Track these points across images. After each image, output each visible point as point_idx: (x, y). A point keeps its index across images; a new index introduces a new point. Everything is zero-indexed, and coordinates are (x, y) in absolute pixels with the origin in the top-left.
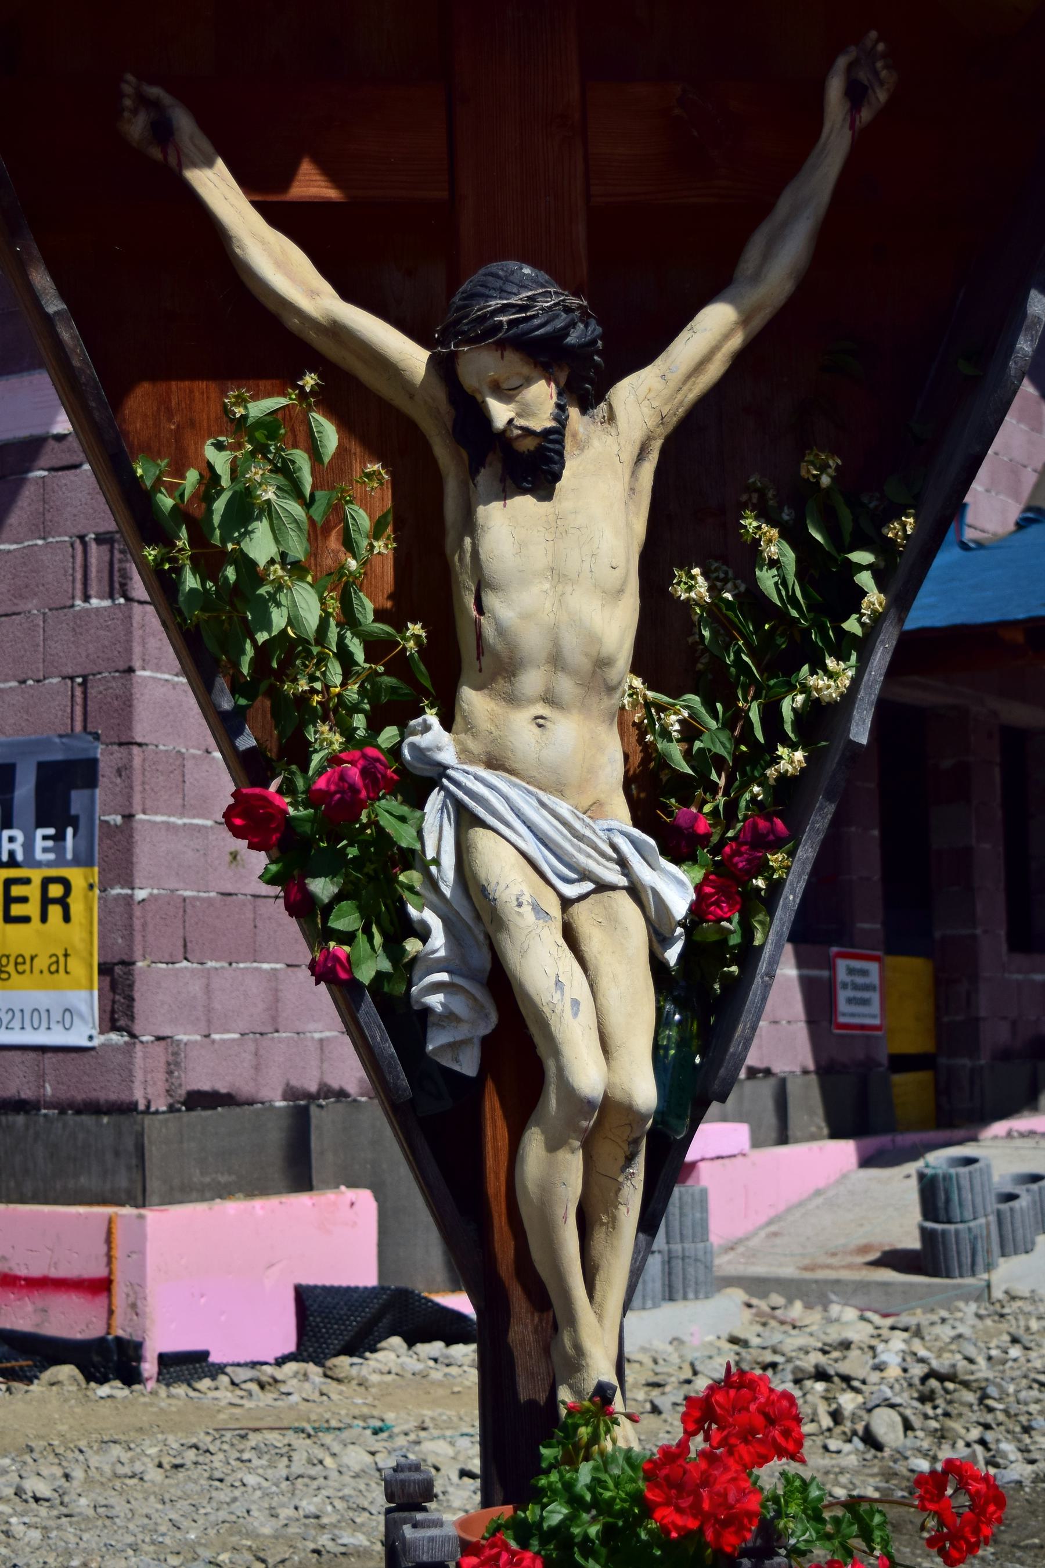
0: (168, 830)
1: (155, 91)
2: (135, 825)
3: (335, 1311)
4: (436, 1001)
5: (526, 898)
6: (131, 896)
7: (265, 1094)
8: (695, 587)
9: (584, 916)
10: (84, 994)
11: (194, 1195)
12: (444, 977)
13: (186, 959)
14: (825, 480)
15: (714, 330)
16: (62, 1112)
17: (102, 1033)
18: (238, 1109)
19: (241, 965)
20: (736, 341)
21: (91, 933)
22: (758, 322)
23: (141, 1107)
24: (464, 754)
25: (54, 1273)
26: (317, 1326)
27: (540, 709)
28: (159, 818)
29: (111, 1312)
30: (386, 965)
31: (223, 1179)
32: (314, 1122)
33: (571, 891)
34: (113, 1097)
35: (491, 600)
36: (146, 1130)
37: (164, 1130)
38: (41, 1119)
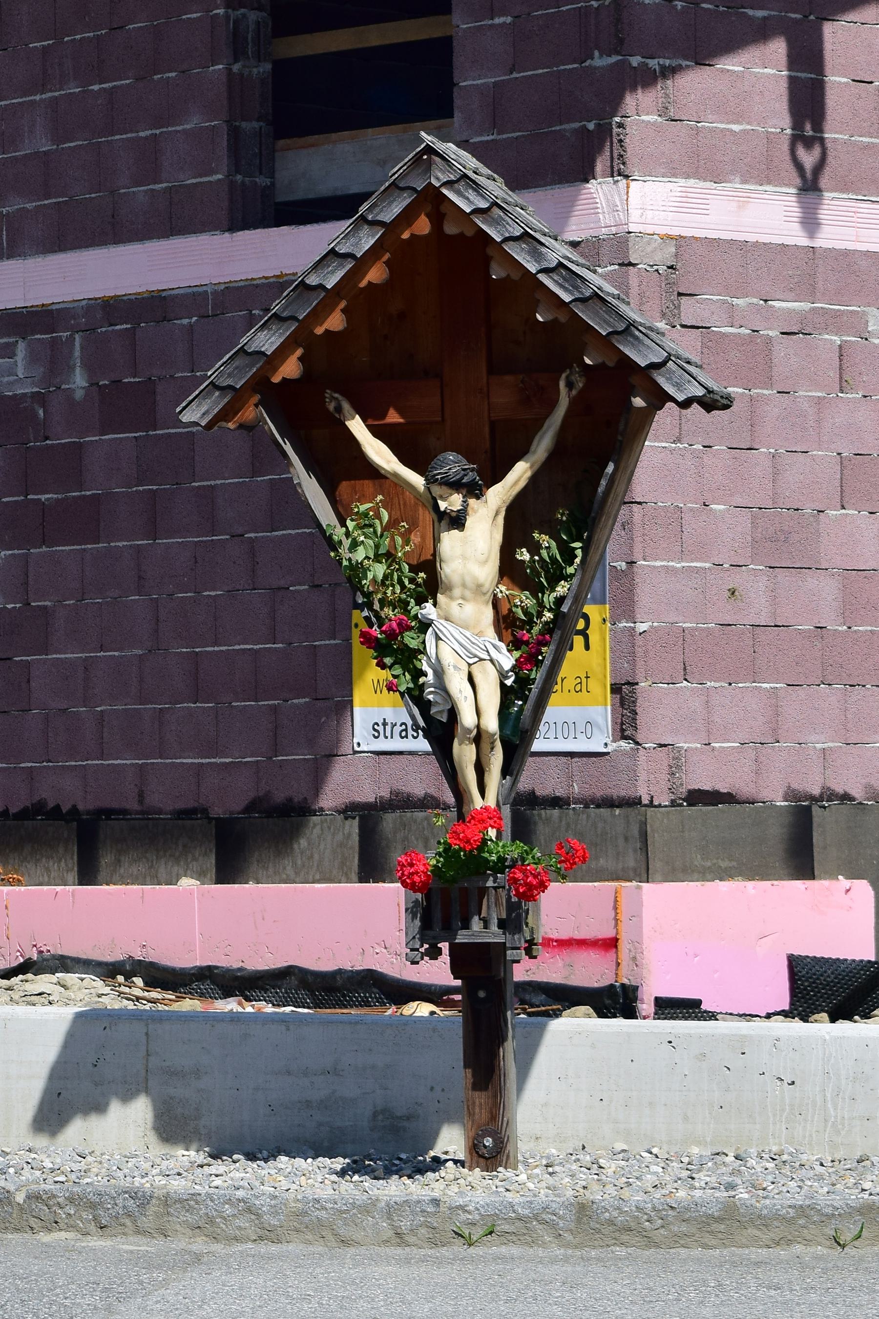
0: (667, 572)
1: (336, 395)
2: (635, 569)
3: (822, 978)
4: (431, 697)
5: (452, 664)
6: (633, 629)
7: (766, 794)
8: (524, 555)
9: (475, 670)
10: (600, 708)
11: (696, 875)
12: (432, 689)
13: (686, 680)
14: (564, 518)
15: (520, 473)
16: (587, 806)
17: (614, 741)
18: (738, 806)
19: (740, 685)
20: (529, 474)
21: (605, 659)
22: (536, 467)
23: (645, 801)
24: (439, 615)
25: (578, 935)
26: (805, 989)
27: (460, 601)
28: (658, 563)
29: (618, 964)
30: (411, 685)
31: (724, 864)
32: (816, 820)
33: (471, 661)
34: (623, 793)
35: (443, 565)
36: (648, 821)
37: (665, 821)
38: (571, 812)
